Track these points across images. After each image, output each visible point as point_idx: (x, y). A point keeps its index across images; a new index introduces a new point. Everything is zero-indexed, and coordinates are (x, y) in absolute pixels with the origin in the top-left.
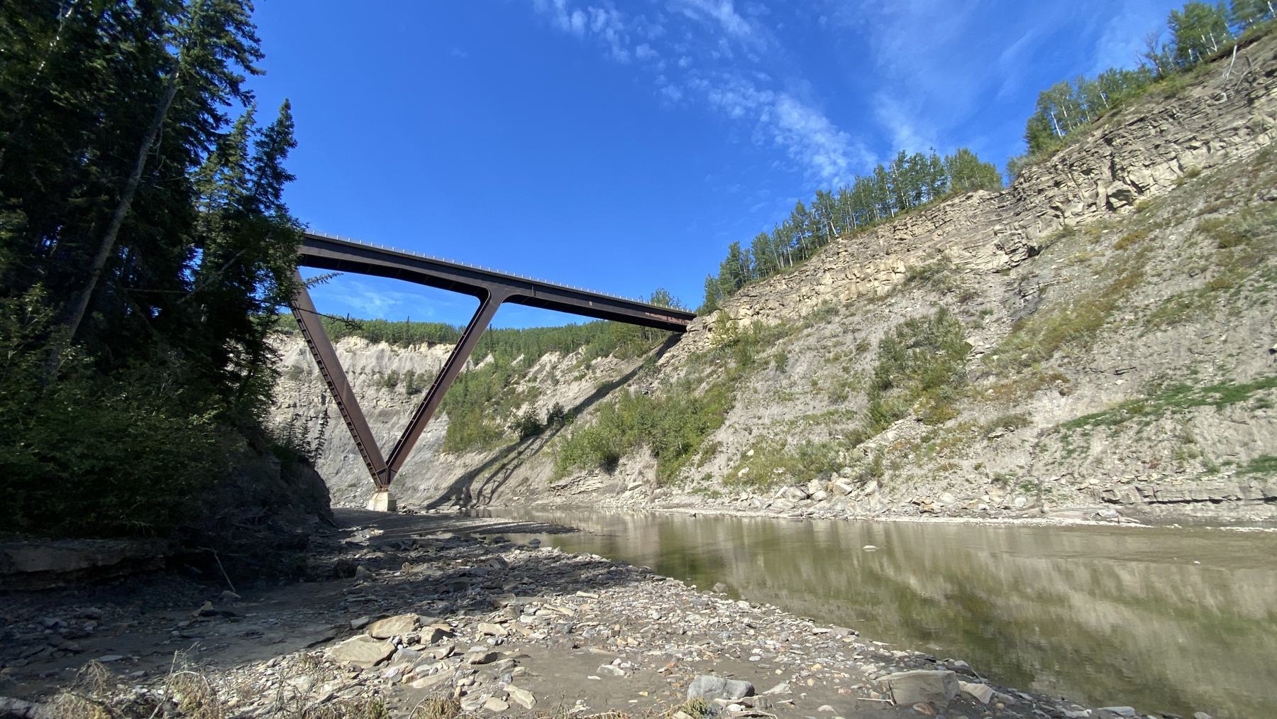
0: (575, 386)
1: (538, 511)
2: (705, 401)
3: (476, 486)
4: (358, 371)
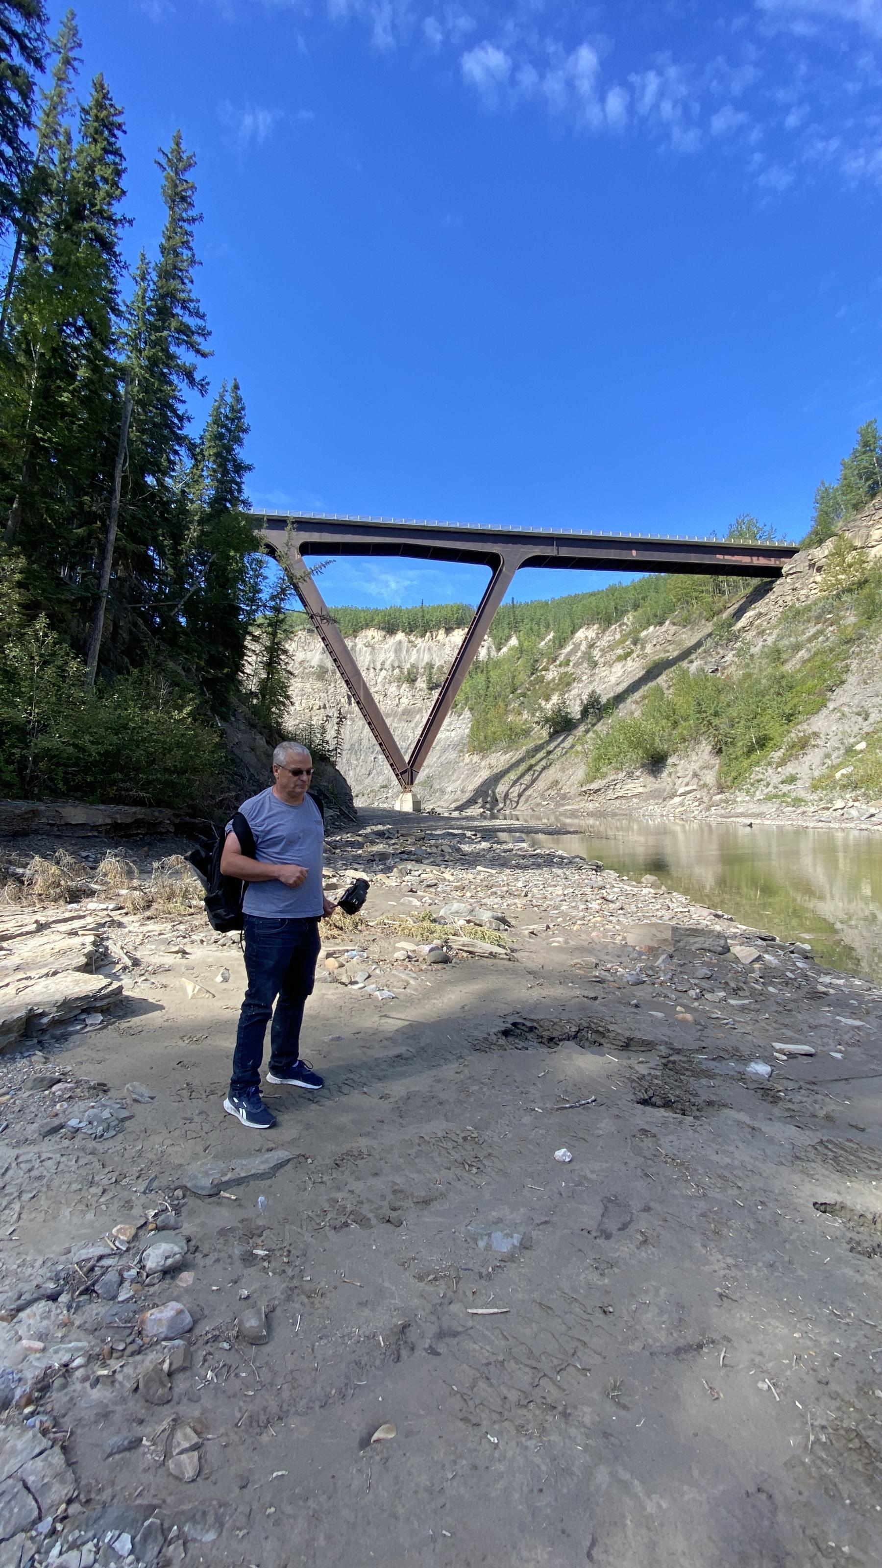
0: (618, 669)
1: (567, 817)
2: (799, 676)
3: (501, 789)
4: (379, 667)
